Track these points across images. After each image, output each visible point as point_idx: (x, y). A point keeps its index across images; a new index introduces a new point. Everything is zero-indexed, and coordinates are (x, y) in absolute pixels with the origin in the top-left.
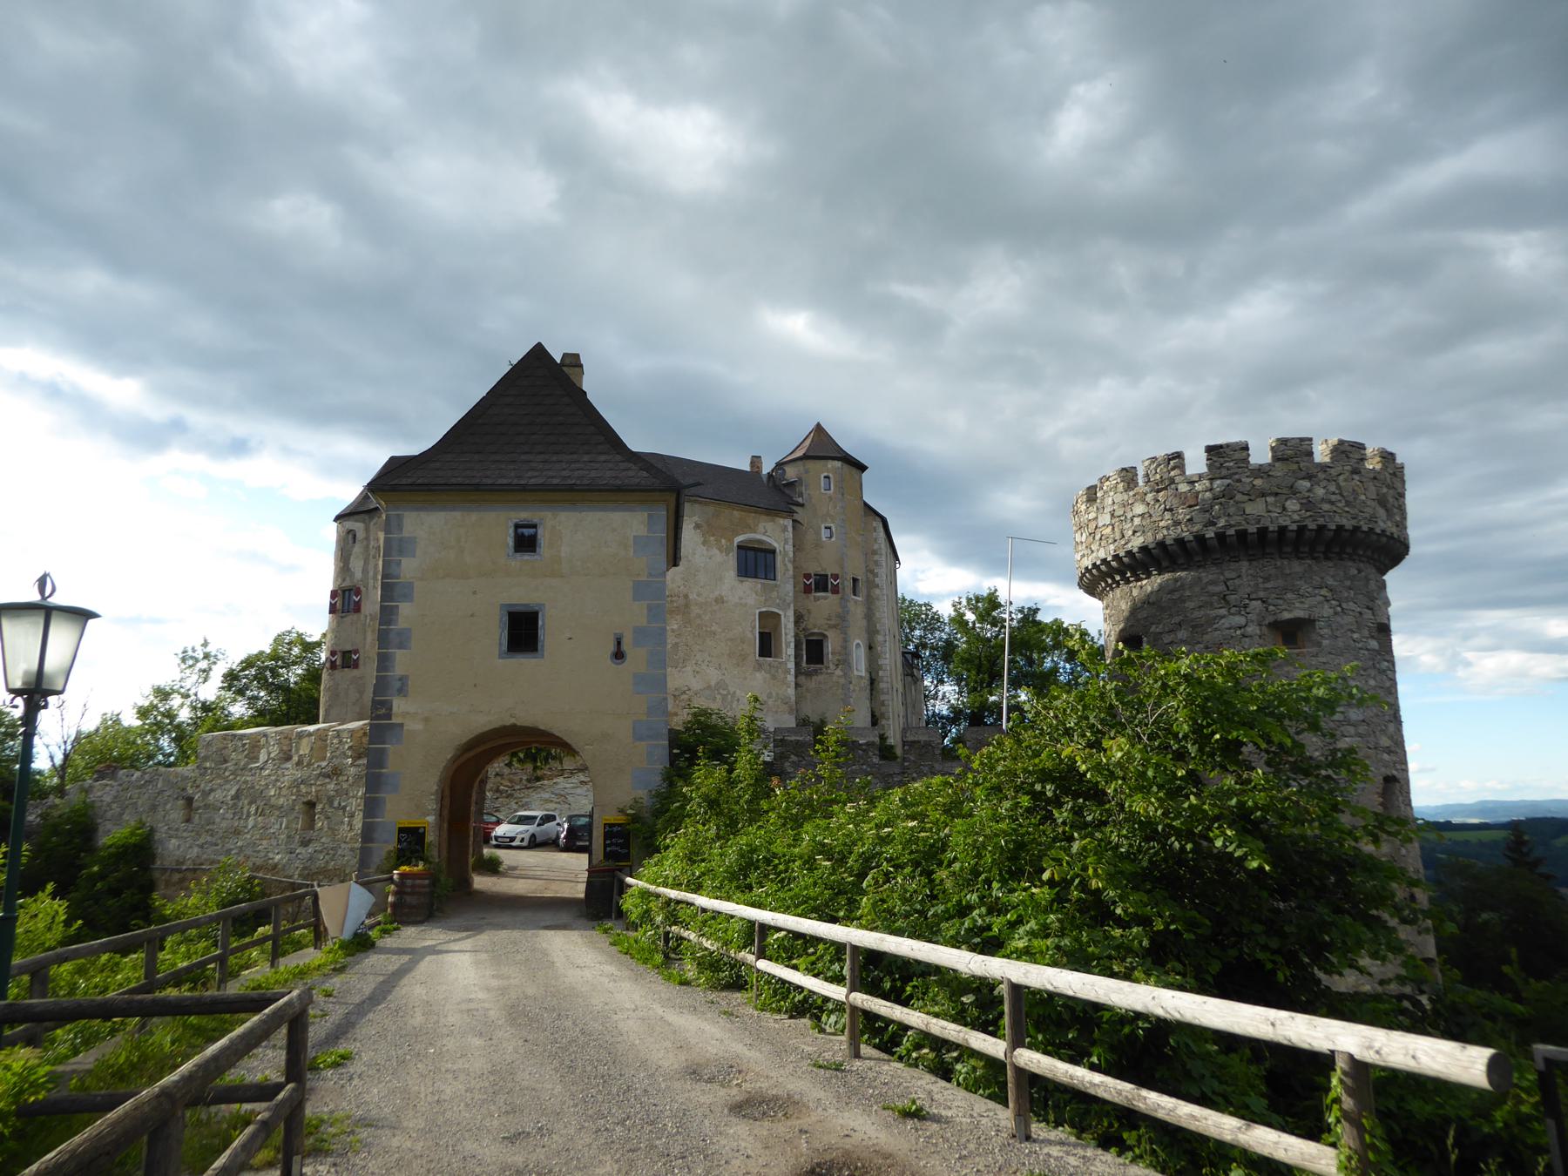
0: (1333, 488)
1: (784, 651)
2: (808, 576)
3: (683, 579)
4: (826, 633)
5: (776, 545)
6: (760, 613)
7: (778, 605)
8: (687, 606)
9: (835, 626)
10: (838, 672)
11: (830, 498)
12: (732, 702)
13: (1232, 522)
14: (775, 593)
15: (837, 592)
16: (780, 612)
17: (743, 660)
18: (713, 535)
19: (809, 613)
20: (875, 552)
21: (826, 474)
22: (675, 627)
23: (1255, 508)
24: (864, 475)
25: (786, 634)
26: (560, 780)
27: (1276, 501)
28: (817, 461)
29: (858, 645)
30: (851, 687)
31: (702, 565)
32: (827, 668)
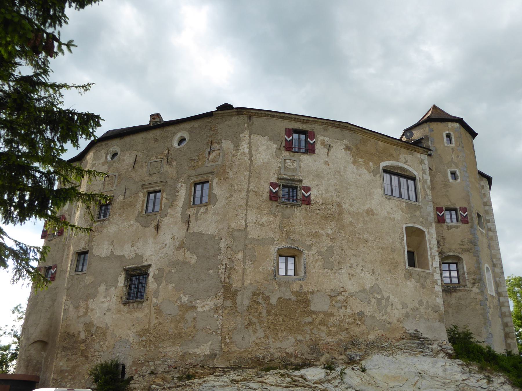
3: (336, 190)
4: (460, 255)
5: (416, 173)
7: (422, 222)
8: (340, 214)
9: (468, 250)
10: (475, 290)
11: (453, 149)
12: (386, 307)
16: (424, 229)
17: (395, 267)
18: (362, 158)
19: (444, 239)
21: (447, 132)
22: (330, 232)
24: (475, 141)
25: (431, 249)
26: (212, 378)
28: (439, 123)
30: (488, 303)
31: (353, 180)
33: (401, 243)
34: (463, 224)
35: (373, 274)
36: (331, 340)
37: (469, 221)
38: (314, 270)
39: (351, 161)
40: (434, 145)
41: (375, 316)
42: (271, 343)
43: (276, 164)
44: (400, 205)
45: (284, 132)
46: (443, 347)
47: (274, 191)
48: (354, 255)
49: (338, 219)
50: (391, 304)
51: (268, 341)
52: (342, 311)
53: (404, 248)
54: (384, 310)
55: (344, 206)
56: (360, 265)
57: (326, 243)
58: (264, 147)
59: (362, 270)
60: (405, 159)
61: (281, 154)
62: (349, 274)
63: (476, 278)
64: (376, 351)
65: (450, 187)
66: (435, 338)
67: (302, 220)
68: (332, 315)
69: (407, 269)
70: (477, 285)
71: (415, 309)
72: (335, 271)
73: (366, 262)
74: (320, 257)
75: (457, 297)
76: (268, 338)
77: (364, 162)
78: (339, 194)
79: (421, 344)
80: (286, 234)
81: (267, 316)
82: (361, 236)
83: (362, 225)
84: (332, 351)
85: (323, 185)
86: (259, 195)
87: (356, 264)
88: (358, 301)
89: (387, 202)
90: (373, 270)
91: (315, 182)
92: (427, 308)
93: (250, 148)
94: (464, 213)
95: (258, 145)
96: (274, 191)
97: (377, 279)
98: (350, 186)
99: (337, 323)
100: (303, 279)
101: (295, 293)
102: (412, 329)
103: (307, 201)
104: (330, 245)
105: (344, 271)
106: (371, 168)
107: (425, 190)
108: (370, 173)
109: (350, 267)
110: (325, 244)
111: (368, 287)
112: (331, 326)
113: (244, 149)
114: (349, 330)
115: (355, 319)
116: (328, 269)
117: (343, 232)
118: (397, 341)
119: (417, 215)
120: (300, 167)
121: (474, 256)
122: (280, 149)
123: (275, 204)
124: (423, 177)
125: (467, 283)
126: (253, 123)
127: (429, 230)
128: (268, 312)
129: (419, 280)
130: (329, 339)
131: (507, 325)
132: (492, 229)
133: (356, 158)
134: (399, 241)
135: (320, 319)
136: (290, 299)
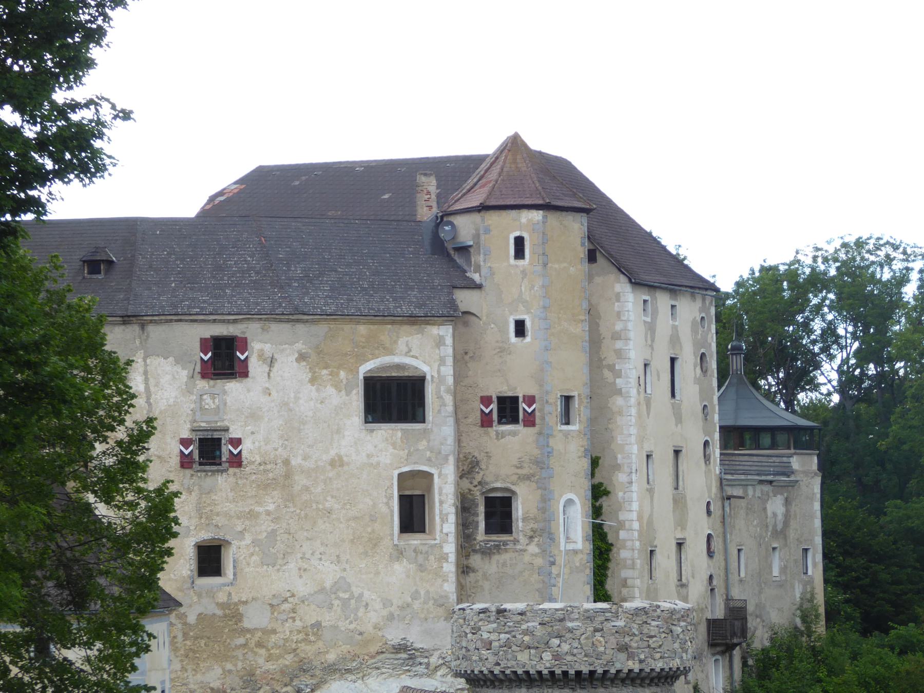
0: (576, 644)
1: (438, 528)
2: (486, 401)
3: (281, 437)
4: (513, 488)
5: (425, 368)
6: (400, 475)
8: (288, 476)
9: (528, 478)
10: (533, 548)
11: (524, 273)
12: (357, 609)
13: (509, 665)
14: (424, 442)
15: (533, 424)
17: (375, 545)
18: (326, 368)
19: (489, 457)
20: (616, 336)
21: (517, 234)
22: (271, 507)
23: (523, 657)
25: (441, 503)
27: (536, 653)
29: (570, 502)
30: (554, 570)
31: (310, 414)
32: (516, 541)
33: (387, 504)
34: (526, 428)
35: (338, 562)
36: (271, 667)
37: (537, 421)
38: (247, 570)
39: (308, 379)
40: (489, 265)
41: (338, 626)
42: (190, 677)
43: (187, 405)
44: (392, 437)
45: (197, 345)
46: (446, 660)
47: (186, 452)
48: (308, 539)
49: (284, 485)
50: (364, 603)
51: (186, 675)
52: (287, 625)
53: (392, 511)
54: (352, 615)
55: (293, 463)
56: (318, 553)
57: (265, 526)
58: (168, 377)
59: (320, 559)
60: (407, 345)
61: (195, 385)
62: (300, 569)
63: (536, 527)
64: (337, 676)
65: (509, 354)
66: (436, 647)
67: (229, 494)
68: (274, 632)
69: (395, 545)
70: (536, 539)
71: (405, 607)
72: (279, 567)
73: (327, 545)
74: (257, 549)
75: (501, 561)
76: (186, 670)
77: (330, 375)
78: (286, 442)
79: (409, 659)
80: (207, 518)
81: (184, 640)
82: (321, 506)
83: (323, 487)
84: (273, 682)
85: (262, 432)
86: (165, 461)
87: (311, 552)
88: (313, 607)
89: (369, 438)
90: (338, 556)
91: (249, 428)
92: (425, 603)
93: (146, 381)
94: (529, 406)
95: (159, 375)
96: (186, 452)
97: (345, 570)
98: (304, 424)
99: (281, 643)
100: (232, 583)
101: (222, 606)
102: (397, 638)
103: (236, 461)
104: (271, 528)
105: (292, 565)
106: (342, 381)
107: (440, 397)
108: (340, 391)
109: (302, 558)
110: (263, 527)
111: (328, 584)
112: (272, 648)
113: (137, 386)
114: (298, 651)
115: (307, 635)
116: (268, 565)
117: (291, 505)
118: (372, 657)
119: (420, 448)
120: (225, 404)
121: (538, 488)
122: (193, 377)
123: (188, 472)
124: (439, 372)
125: (521, 537)
126: (148, 337)
127: (441, 471)
128: (185, 635)
129: (416, 558)
130: (270, 666)
131: (626, 583)
132: (623, 390)
133: (317, 370)
134: (385, 500)
135: (257, 639)
136: (214, 614)
